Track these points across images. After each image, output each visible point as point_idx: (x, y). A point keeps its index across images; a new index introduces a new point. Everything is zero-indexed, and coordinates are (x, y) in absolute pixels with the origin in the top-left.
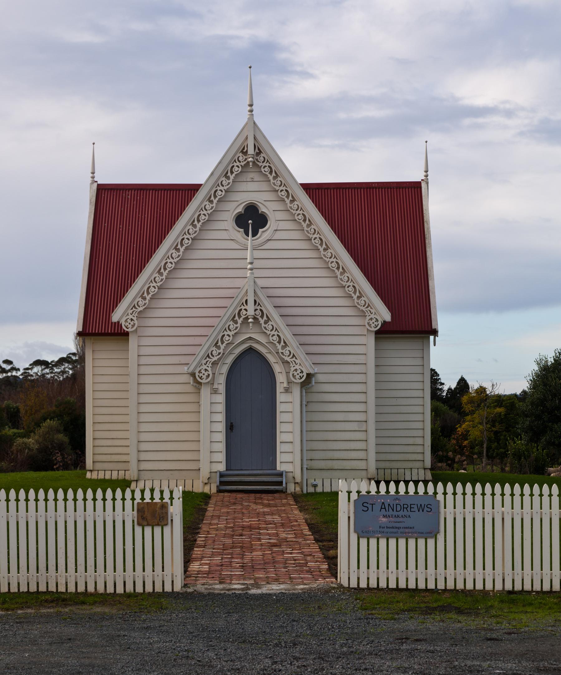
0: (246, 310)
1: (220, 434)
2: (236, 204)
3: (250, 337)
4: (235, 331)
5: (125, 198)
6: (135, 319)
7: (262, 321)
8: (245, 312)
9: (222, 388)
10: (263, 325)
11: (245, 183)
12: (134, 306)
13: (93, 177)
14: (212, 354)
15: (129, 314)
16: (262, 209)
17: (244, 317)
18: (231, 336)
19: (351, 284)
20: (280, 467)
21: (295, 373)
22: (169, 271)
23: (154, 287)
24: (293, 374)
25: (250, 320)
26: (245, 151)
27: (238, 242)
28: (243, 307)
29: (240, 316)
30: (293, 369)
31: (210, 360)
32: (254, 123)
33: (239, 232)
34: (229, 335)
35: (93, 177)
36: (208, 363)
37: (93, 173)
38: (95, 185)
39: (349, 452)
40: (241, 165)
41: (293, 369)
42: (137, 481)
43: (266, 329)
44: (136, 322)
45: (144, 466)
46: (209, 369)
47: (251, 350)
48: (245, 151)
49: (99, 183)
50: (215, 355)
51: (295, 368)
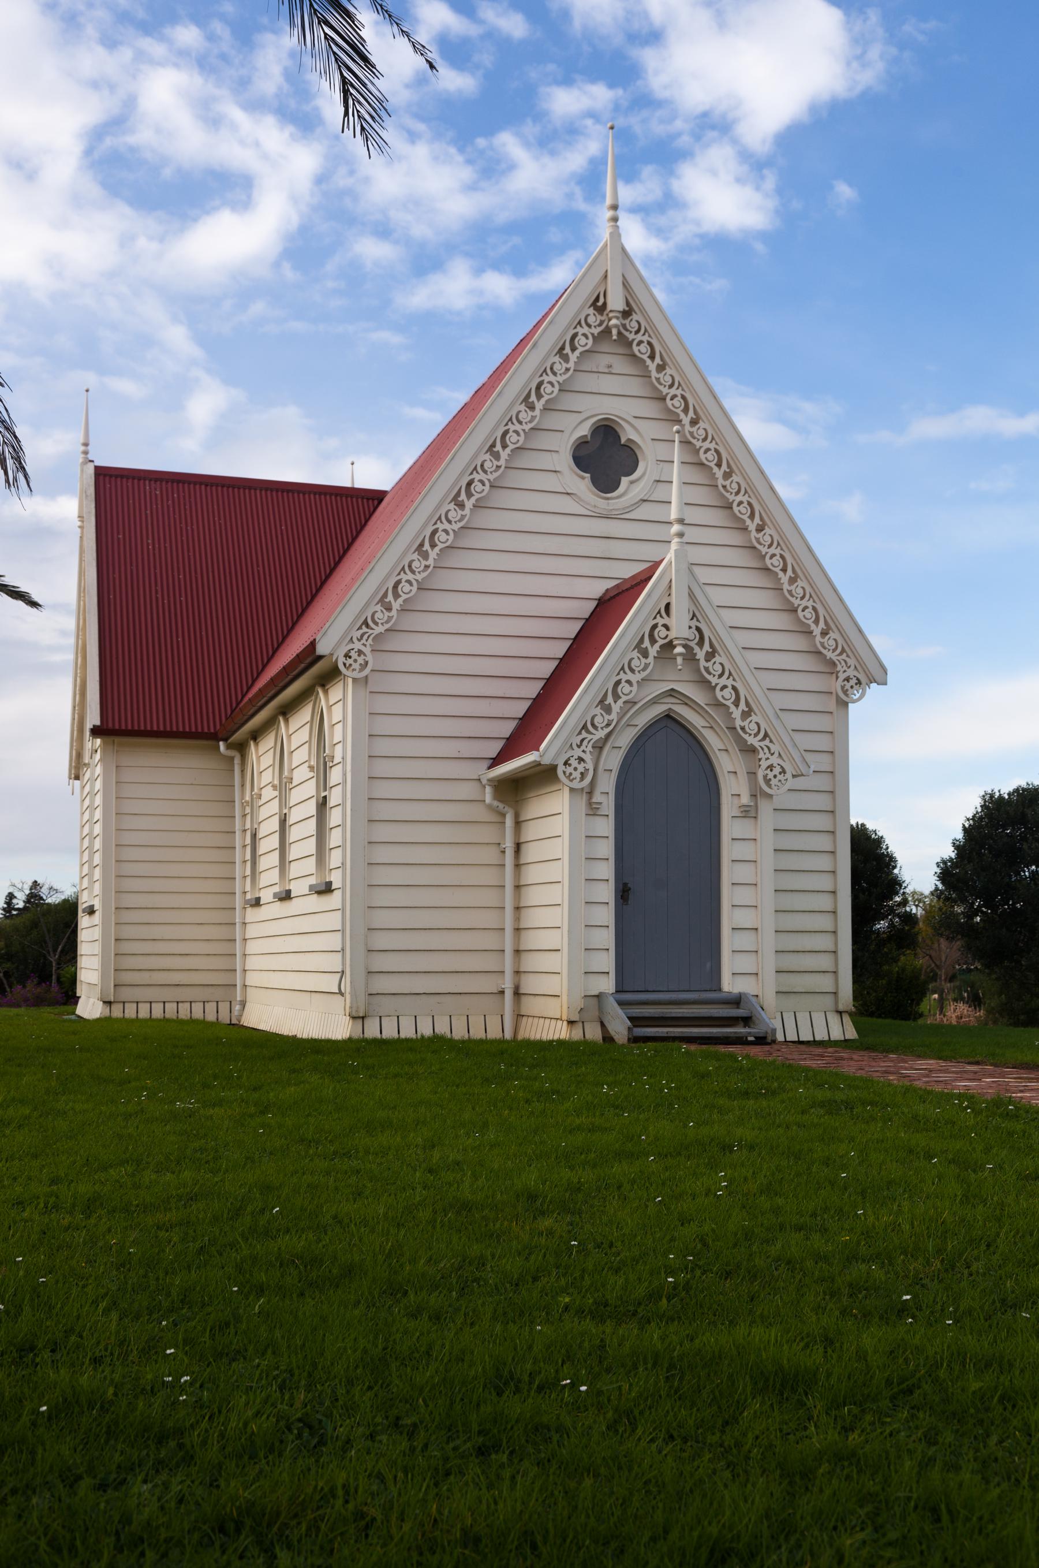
0: (667, 627)
1: (603, 909)
2: (576, 418)
3: (672, 690)
4: (644, 674)
5: (150, 493)
6: (367, 650)
7: (701, 655)
8: (663, 632)
9: (608, 804)
10: (703, 663)
11: (596, 375)
12: (366, 623)
13: (86, 453)
14: (593, 725)
15: (355, 639)
16: (628, 434)
17: (661, 642)
18: (635, 684)
19: (810, 604)
20: (730, 985)
21: (770, 775)
22: (441, 550)
23: (409, 582)
24: (765, 777)
25: (679, 650)
26: (600, 304)
27: (580, 498)
28: (660, 621)
29: (653, 641)
30: (764, 764)
31: (590, 737)
32: (623, 250)
33: (583, 478)
34: (629, 682)
35: (86, 453)
36: (585, 743)
37: (86, 444)
38: (90, 470)
39: (800, 954)
40: (593, 334)
41: (764, 764)
42: (363, 1018)
43: (709, 673)
44: (370, 658)
45: (383, 984)
46: (587, 757)
47: (669, 718)
48: (600, 304)
49: (97, 464)
50: (599, 726)
51: (769, 763)
